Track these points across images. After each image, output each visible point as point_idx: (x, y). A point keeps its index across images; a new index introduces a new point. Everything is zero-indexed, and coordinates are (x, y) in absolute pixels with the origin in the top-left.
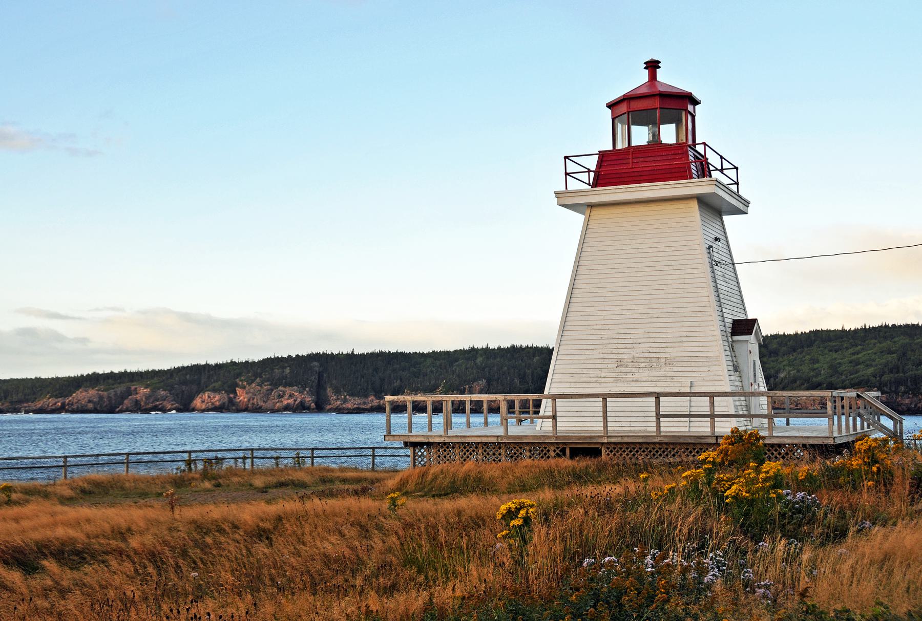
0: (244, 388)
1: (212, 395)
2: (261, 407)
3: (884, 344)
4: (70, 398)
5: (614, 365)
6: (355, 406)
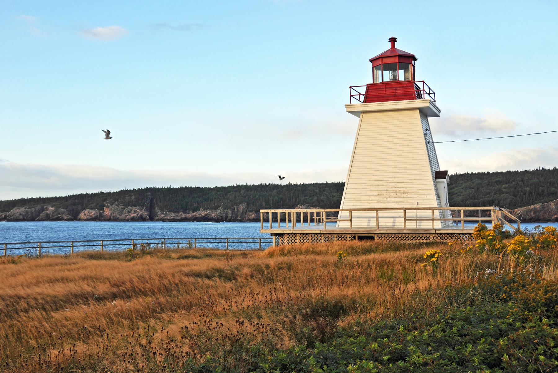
0: (108, 207)
1: (90, 211)
2: (118, 218)
3: (467, 184)
4: (10, 213)
5: (377, 194)
6: (172, 218)
